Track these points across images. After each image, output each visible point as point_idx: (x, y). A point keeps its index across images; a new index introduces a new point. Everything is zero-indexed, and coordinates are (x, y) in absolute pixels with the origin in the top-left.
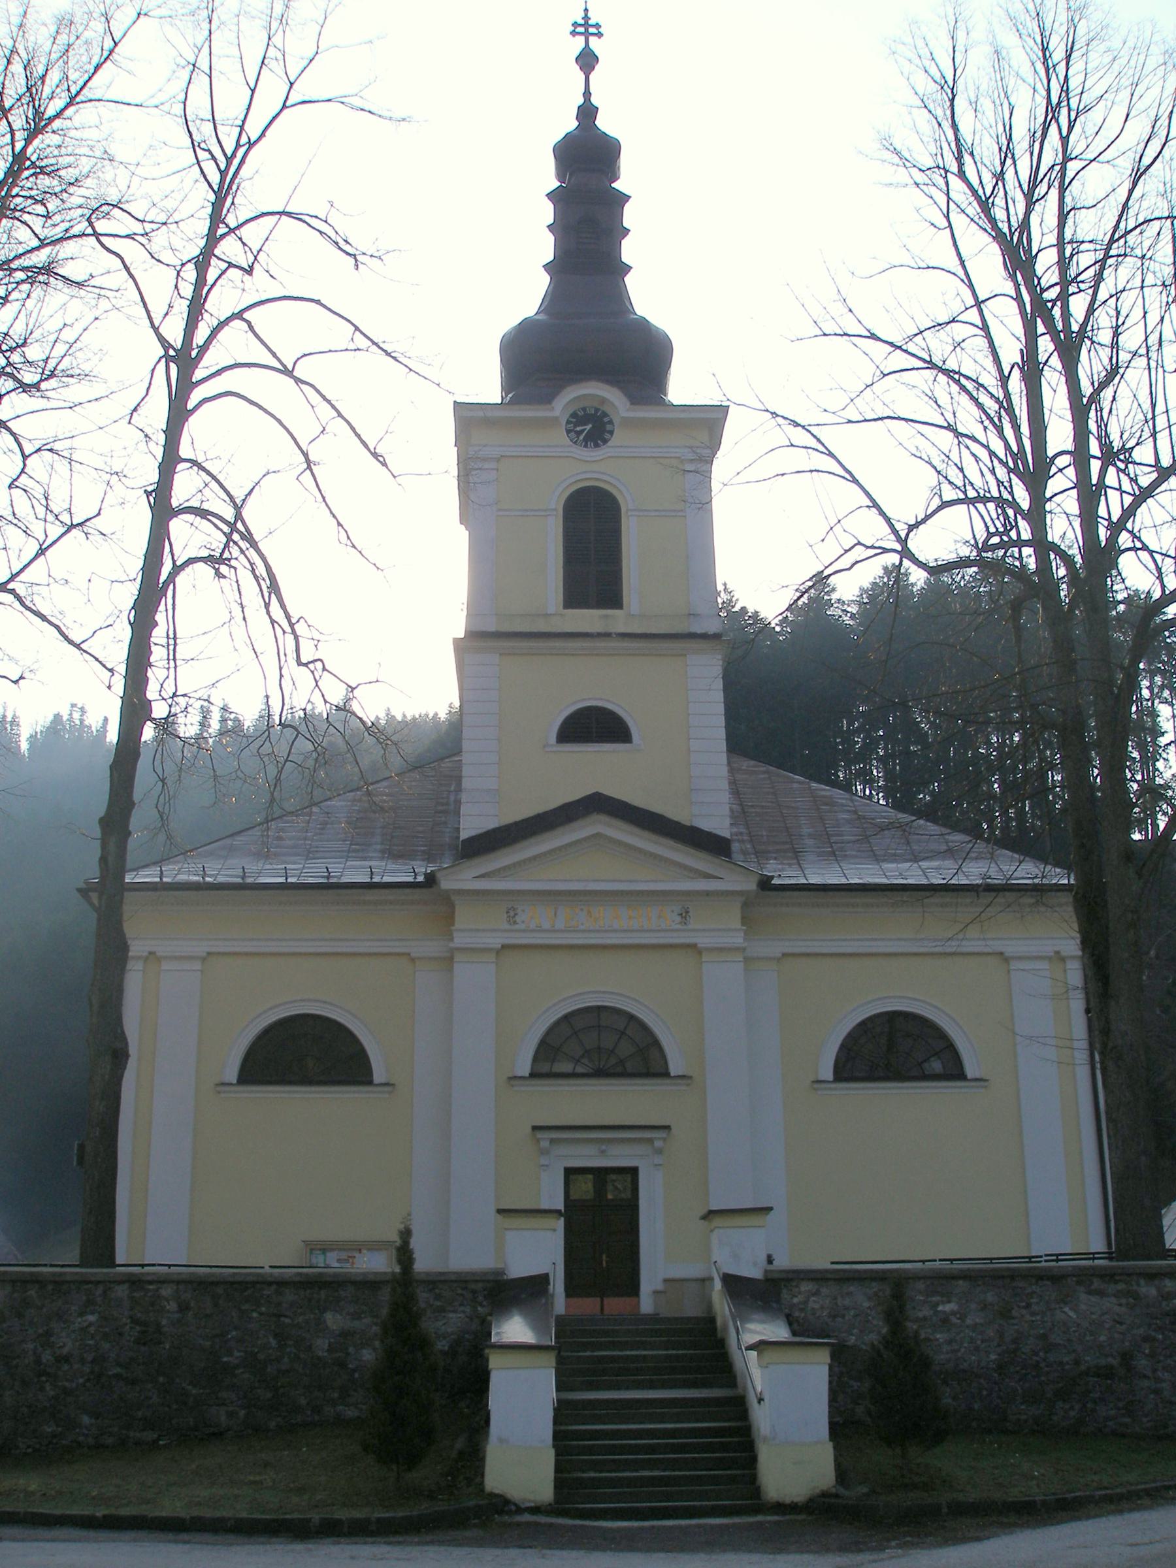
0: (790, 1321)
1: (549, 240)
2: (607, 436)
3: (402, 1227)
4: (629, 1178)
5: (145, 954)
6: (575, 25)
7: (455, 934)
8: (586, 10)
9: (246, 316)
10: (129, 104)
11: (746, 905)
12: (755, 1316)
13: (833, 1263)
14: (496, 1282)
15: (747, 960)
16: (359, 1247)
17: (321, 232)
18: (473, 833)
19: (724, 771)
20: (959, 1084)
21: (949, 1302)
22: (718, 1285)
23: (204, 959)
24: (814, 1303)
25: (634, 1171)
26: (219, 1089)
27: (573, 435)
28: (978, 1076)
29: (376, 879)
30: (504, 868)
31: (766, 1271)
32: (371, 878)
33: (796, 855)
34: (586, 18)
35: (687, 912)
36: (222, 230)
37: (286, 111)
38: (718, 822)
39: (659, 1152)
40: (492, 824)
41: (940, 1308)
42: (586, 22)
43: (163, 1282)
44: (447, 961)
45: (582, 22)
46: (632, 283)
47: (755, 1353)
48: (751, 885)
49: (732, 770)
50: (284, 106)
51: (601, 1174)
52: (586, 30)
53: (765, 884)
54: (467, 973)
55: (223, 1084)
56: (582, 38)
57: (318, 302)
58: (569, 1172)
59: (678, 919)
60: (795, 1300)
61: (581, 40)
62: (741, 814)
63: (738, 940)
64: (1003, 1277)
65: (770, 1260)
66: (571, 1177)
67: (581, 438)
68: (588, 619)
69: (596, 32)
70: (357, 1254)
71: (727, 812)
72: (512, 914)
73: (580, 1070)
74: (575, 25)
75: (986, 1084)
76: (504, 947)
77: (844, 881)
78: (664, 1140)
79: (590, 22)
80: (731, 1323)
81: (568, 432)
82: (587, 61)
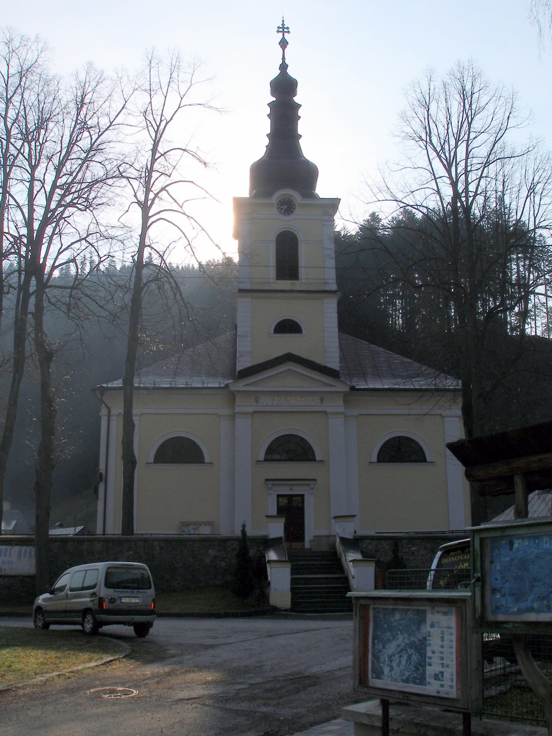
0: (362, 553)
1: (268, 122)
2: (293, 210)
3: (243, 524)
4: (300, 498)
5: (117, 414)
6: (279, 28)
7: (236, 407)
8: (283, 21)
9: (166, 189)
10: (132, 126)
11: (345, 395)
12: (351, 551)
13: (376, 533)
14: (265, 539)
15: (346, 417)
16: (200, 524)
17: (193, 155)
18: (242, 368)
19: (337, 340)
20: (424, 464)
21: (415, 546)
22: (338, 540)
23: (140, 416)
24: (370, 547)
25: (302, 496)
26: (147, 465)
27: (279, 210)
28: (431, 461)
29: (205, 386)
30: (254, 382)
31: (354, 536)
32: (203, 385)
33: (364, 376)
34: (283, 25)
35: (323, 399)
36: (158, 155)
37: (180, 109)
38: (334, 363)
39: (312, 489)
40: (249, 364)
41: (411, 549)
42: (283, 26)
43: (154, 540)
44: (233, 416)
45: (282, 26)
46: (302, 142)
47: (352, 563)
48: (347, 389)
49: (340, 339)
50: (179, 107)
51: (290, 497)
52: (283, 30)
53: (353, 389)
54: (239, 421)
55: (148, 463)
56: (282, 34)
57: (192, 182)
58: (278, 496)
59: (319, 401)
60: (364, 546)
61: (281, 34)
62: (343, 358)
63: (342, 409)
64: (432, 539)
65: (355, 532)
66: (280, 498)
67: (283, 211)
68: (286, 284)
69: (287, 31)
70: (200, 527)
71: (338, 356)
72: (257, 399)
73: (282, 458)
74: (279, 28)
75: (434, 464)
76: (254, 412)
77: (382, 387)
78: (314, 484)
79: (285, 27)
80: (343, 553)
81: (278, 208)
82: (284, 44)
